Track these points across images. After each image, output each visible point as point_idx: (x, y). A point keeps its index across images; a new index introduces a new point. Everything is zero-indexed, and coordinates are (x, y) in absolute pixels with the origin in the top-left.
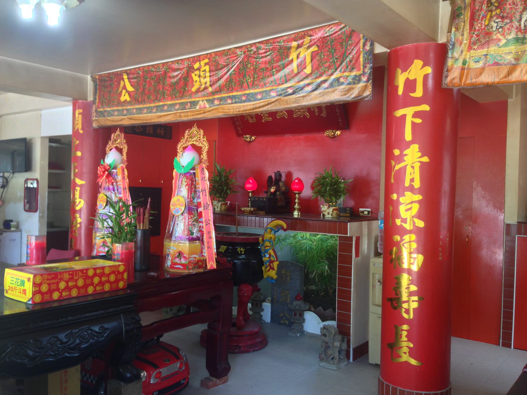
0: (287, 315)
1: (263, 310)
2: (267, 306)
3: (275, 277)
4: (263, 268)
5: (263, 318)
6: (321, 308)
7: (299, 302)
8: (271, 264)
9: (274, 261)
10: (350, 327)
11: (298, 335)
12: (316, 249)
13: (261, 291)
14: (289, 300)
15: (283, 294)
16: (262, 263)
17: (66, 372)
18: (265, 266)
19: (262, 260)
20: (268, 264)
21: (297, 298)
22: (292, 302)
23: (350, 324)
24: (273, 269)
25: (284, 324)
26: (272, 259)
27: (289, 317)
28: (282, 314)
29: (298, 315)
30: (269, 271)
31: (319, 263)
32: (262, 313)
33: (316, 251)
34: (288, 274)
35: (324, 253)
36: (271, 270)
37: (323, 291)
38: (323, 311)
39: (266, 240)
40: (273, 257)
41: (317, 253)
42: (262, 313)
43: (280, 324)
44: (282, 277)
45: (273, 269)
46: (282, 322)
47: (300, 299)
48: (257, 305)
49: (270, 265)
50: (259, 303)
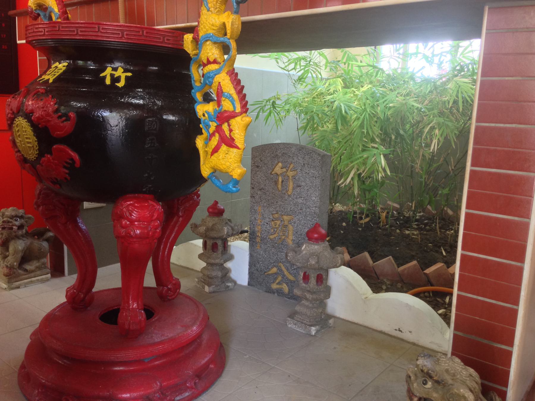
0: (286, 273)
1: (231, 258)
2: (240, 248)
3: (237, 171)
4: (200, 142)
5: (233, 275)
6: (366, 254)
7: (316, 247)
8: (225, 127)
9: (233, 115)
10: (510, 354)
11: (313, 330)
12: (358, 119)
13: (226, 215)
14: (291, 237)
15: (278, 222)
16: (193, 126)
17: (336, 193)
18: (205, 134)
19: (194, 113)
20: (213, 125)
21: (312, 235)
22: (299, 245)
23: (511, 344)
24: (230, 143)
25: (280, 292)
26: (227, 105)
27: (291, 278)
28: (275, 270)
29: (313, 281)
30: (216, 150)
31: (363, 150)
32: (228, 265)
33: (357, 123)
34: (290, 174)
35: (377, 130)
36: (224, 148)
37: (367, 216)
38: (370, 261)
39: (207, 38)
40: (230, 97)
41: (362, 126)
42: (228, 265)
43: (270, 291)
44: (276, 183)
45: (230, 143)
46: (274, 286)
47: (322, 238)
48: (215, 247)
49: (219, 129)
50: (219, 243)
